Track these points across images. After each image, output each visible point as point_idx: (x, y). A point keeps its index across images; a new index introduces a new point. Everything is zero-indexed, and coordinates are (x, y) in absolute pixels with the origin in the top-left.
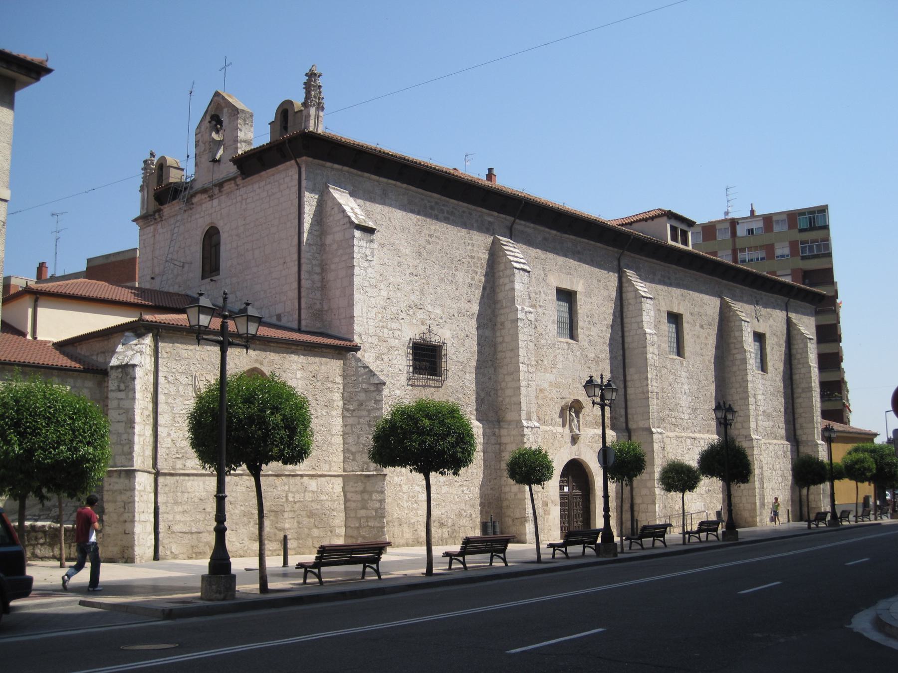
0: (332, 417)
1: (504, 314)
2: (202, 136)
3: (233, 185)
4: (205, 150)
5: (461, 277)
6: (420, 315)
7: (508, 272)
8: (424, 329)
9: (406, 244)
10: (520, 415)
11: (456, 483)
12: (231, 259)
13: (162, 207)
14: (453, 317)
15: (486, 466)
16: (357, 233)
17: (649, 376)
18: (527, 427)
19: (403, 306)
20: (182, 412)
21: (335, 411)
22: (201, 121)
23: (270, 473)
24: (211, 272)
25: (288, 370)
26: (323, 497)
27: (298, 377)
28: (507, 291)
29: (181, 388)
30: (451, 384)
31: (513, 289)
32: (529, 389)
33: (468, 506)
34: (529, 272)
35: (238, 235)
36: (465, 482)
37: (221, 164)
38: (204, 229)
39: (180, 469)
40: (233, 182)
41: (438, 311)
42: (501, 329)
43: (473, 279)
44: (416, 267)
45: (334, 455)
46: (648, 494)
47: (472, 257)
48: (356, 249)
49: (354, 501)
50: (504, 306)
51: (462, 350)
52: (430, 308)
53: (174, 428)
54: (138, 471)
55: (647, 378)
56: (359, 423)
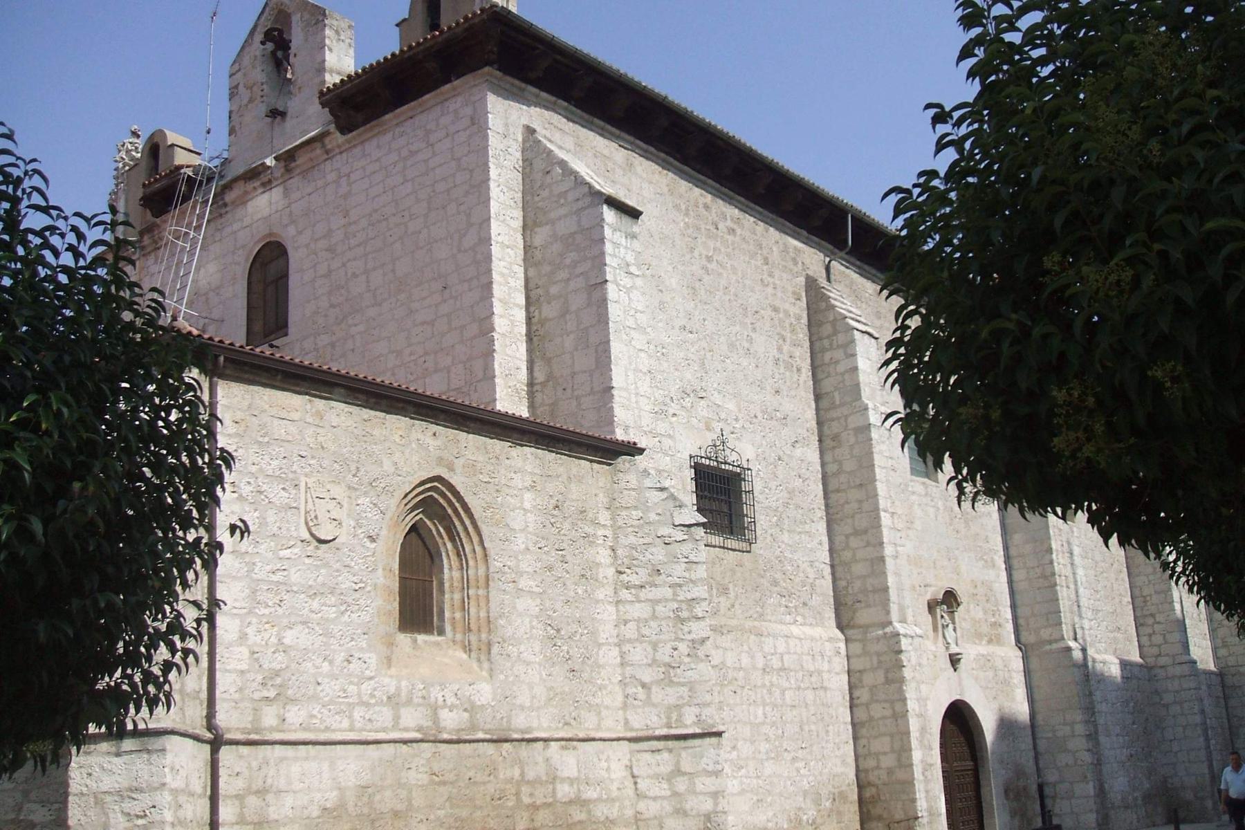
0: (597, 602)
1: (838, 418)
2: (245, 75)
3: (318, 151)
4: (251, 101)
5: (764, 345)
6: (702, 409)
7: (841, 338)
8: (710, 437)
9: (670, 268)
10: (888, 613)
11: (786, 754)
12: (316, 299)
13: (158, 221)
14: (754, 420)
15: (900, 717)
16: (609, 215)
17: (1054, 546)
18: (905, 636)
19: (674, 390)
20: (274, 578)
21: (602, 589)
22: (243, 48)
23: (481, 735)
24: (266, 336)
25: (505, 488)
26: (591, 794)
27: (527, 505)
28: (842, 374)
29: (271, 517)
30: (761, 552)
31: (856, 369)
32: (898, 561)
33: (808, 801)
34: (876, 338)
35: (330, 250)
36: (800, 751)
37: (288, 118)
38: (251, 251)
39: (272, 729)
40: (318, 145)
41: (731, 406)
42: (834, 448)
43: (780, 349)
44: (689, 316)
45: (604, 692)
46: (1071, 762)
47: (776, 310)
48: (608, 247)
49: (655, 799)
50: (838, 403)
51: (773, 484)
52: (717, 398)
53: (254, 620)
54: (172, 732)
55: (1050, 550)
56: (654, 617)
